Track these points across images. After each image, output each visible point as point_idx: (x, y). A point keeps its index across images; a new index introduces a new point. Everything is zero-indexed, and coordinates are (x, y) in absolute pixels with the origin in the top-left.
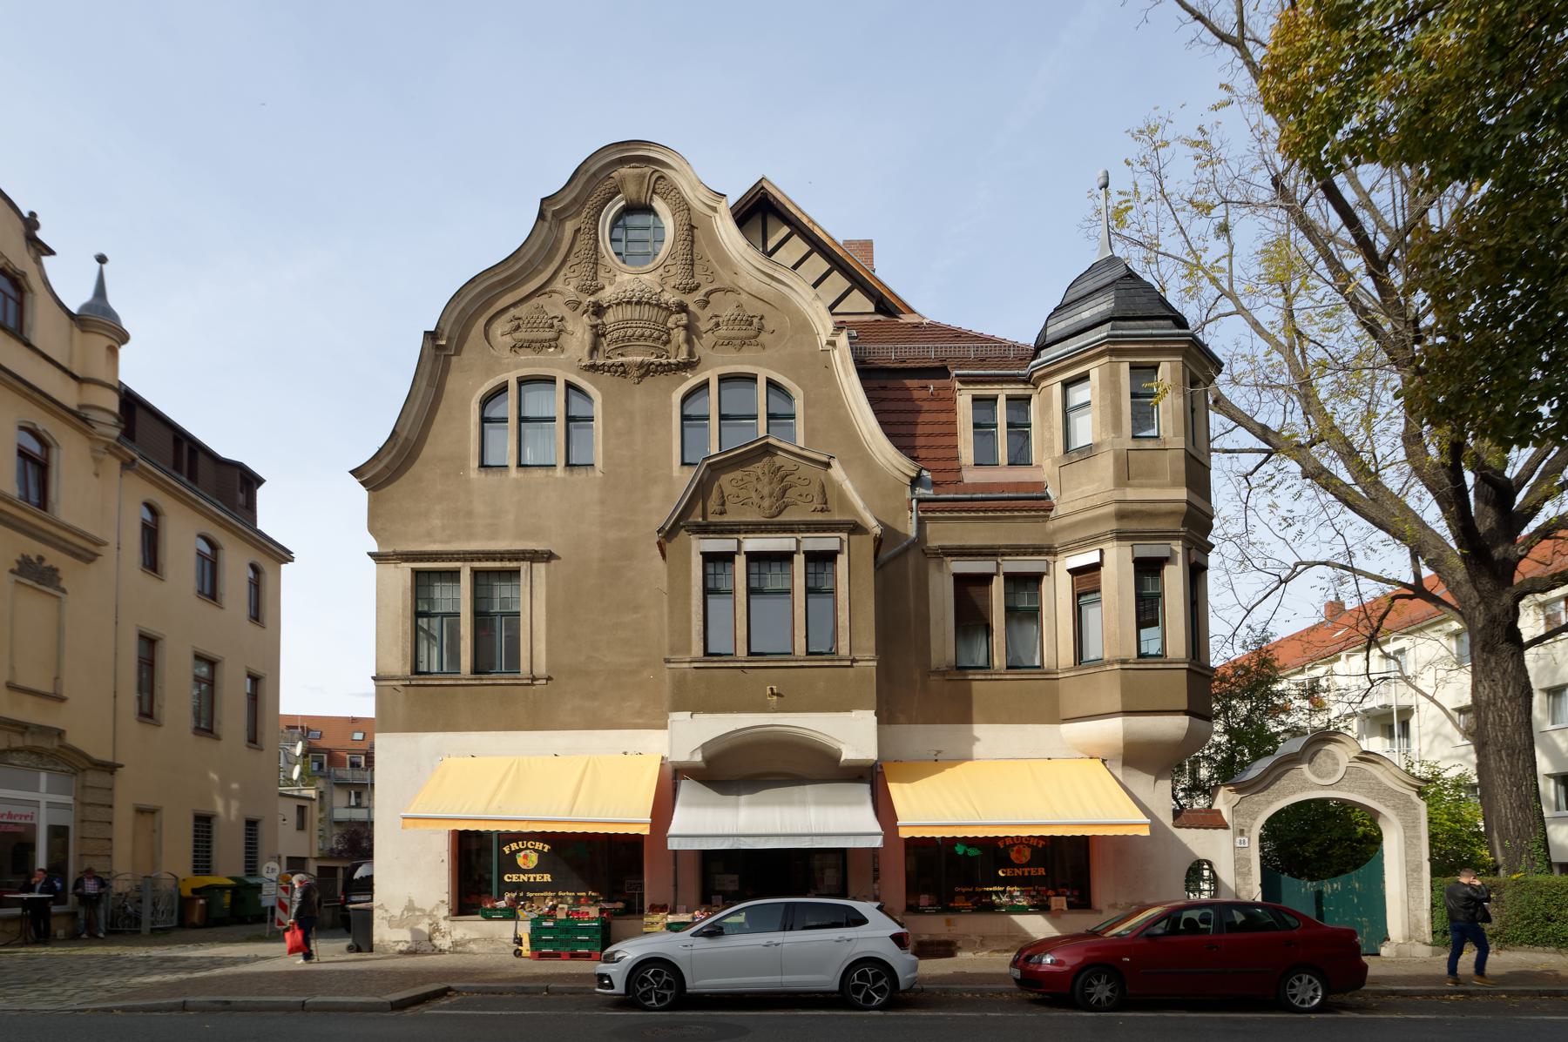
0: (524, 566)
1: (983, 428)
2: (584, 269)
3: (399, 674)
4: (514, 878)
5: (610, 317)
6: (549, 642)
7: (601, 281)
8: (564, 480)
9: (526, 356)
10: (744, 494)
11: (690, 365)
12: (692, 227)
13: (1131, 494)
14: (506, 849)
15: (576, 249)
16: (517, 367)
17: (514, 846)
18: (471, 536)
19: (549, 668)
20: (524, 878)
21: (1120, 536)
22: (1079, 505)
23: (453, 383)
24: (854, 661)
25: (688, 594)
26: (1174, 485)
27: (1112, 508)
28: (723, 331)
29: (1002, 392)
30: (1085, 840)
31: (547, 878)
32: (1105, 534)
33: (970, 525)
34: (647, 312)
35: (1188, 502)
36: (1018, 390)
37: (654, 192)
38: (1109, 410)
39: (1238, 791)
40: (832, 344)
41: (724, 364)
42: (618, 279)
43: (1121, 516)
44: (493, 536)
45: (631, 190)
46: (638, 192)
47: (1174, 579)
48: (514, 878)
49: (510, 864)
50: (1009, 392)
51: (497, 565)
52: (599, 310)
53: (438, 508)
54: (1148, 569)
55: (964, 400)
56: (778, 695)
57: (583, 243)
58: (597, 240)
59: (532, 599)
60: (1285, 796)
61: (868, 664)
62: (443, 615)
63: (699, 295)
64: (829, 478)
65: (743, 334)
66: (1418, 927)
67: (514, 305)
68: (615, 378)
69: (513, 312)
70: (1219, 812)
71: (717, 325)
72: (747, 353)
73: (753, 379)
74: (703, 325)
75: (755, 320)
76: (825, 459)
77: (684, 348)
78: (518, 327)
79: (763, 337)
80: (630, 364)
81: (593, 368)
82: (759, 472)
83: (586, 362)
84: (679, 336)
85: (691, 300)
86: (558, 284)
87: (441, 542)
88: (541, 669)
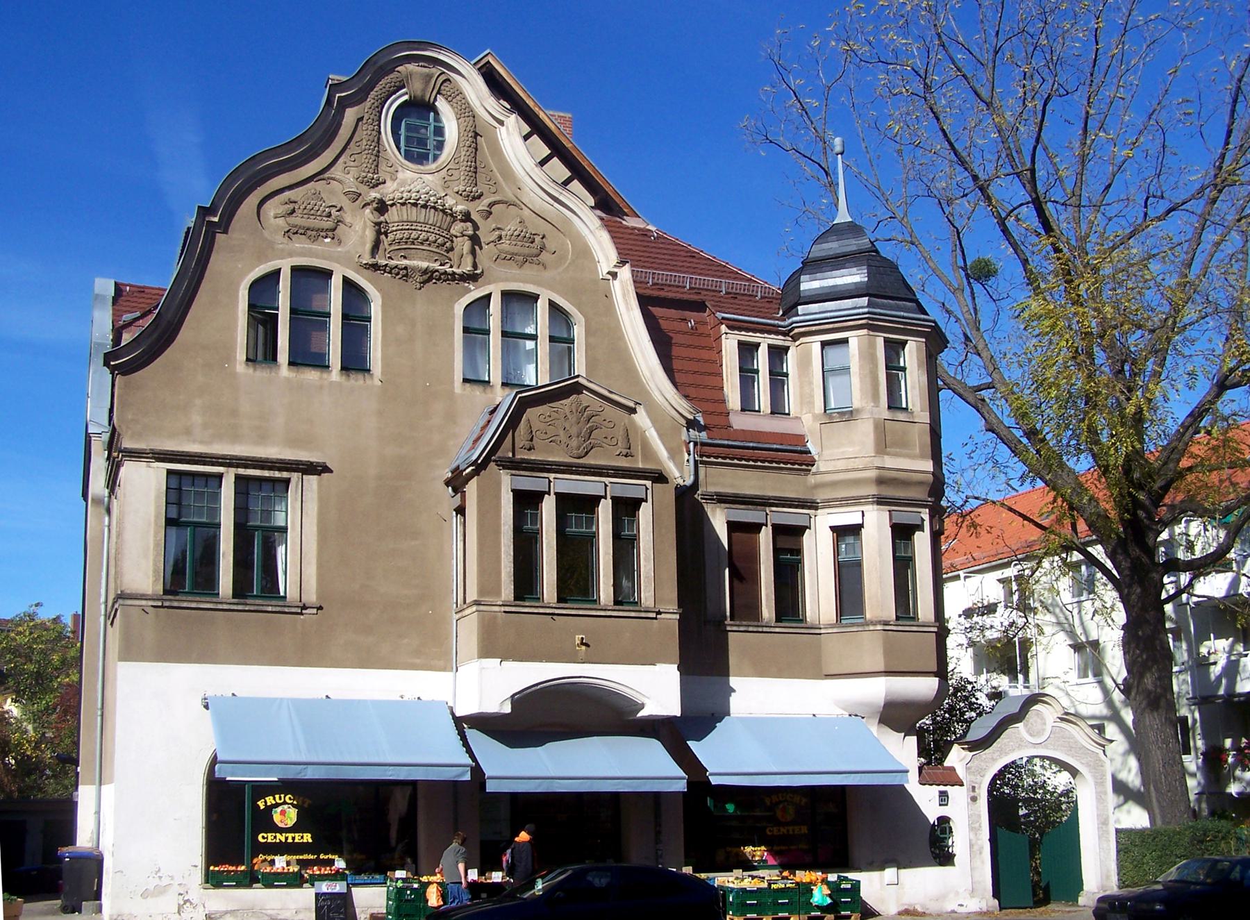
0: (295, 477)
1: (747, 374)
2: (366, 160)
3: (150, 592)
4: (270, 837)
5: (393, 215)
6: (320, 566)
7: (382, 175)
8: (340, 384)
9: (300, 243)
10: (549, 433)
11: (473, 277)
12: (476, 135)
13: (889, 462)
14: (261, 804)
15: (356, 138)
16: (291, 255)
17: (270, 800)
18: (236, 439)
19: (320, 594)
20: (281, 837)
21: (881, 501)
22: (841, 465)
23: (217, 262)
24: (659, 613)
25: (497, 532)
26: (922, 457)
27: (872, 474)
28: (505, 245)
29: (765, 342)
30: (839, 793)
31: (307, 838)
32: (867, 497)
33: (741, 472)
34: (432, 216)
35: (933, 474)
36: (778, 340)
37: (439, 93)
38: (868, 380)
39: (970, 750)
40: (614, 275)
41: (507, 280)
42: (400, 175)
43: (880, 481)
44: (262, 438)
45: (417, 87)
46: (424, 90)
47: (922, 541)
48: (270, 837)
49: (264, 821)
50: (771, 342)
51: (266, 473)
52: (382, 207)
53: (198, 402)
54: (902, 533)
55: (730, 345)
56: (587, 645)
57: (364, 133)
58: (380, 133)
59: (300, 515)
60: (1007, 754)
61: (672, 617)
62: (196, 525)
63: (483, 204)
64: (633, 423)
65: (526, 251)
66: (1108, 877)
67: (291, 187)
68: (397, 281)
69: (287, 194)
70: (952, 769)
71: (500, 238)
72: (529, 271)
73: (535, 298)
74: (484, 236)
75: (538, 239)
76: (632, 404)
77: (468, 260)
78: (293, 211)
79: (545, 256)
80: (414, 269)
81: (375, 267)
82: (567, 410)
83: (367, 259)
84: (464, 245)
85: (476, 209)
86: (336, 172)
87: (201, 442)
88: (311, 597)
